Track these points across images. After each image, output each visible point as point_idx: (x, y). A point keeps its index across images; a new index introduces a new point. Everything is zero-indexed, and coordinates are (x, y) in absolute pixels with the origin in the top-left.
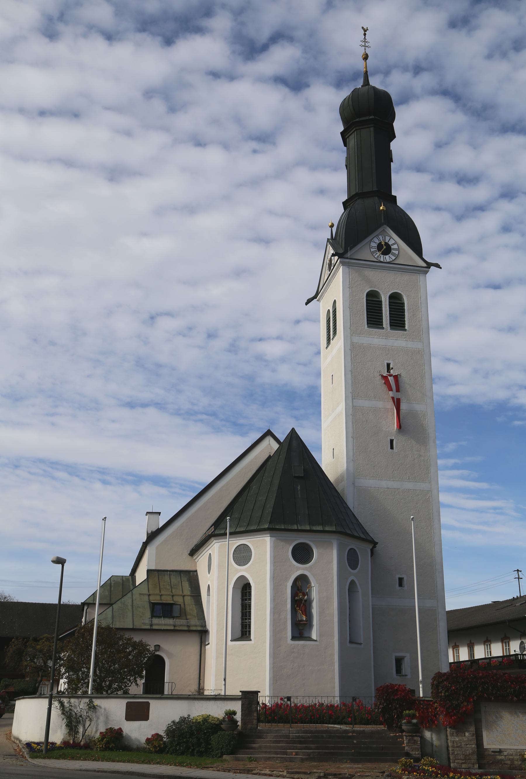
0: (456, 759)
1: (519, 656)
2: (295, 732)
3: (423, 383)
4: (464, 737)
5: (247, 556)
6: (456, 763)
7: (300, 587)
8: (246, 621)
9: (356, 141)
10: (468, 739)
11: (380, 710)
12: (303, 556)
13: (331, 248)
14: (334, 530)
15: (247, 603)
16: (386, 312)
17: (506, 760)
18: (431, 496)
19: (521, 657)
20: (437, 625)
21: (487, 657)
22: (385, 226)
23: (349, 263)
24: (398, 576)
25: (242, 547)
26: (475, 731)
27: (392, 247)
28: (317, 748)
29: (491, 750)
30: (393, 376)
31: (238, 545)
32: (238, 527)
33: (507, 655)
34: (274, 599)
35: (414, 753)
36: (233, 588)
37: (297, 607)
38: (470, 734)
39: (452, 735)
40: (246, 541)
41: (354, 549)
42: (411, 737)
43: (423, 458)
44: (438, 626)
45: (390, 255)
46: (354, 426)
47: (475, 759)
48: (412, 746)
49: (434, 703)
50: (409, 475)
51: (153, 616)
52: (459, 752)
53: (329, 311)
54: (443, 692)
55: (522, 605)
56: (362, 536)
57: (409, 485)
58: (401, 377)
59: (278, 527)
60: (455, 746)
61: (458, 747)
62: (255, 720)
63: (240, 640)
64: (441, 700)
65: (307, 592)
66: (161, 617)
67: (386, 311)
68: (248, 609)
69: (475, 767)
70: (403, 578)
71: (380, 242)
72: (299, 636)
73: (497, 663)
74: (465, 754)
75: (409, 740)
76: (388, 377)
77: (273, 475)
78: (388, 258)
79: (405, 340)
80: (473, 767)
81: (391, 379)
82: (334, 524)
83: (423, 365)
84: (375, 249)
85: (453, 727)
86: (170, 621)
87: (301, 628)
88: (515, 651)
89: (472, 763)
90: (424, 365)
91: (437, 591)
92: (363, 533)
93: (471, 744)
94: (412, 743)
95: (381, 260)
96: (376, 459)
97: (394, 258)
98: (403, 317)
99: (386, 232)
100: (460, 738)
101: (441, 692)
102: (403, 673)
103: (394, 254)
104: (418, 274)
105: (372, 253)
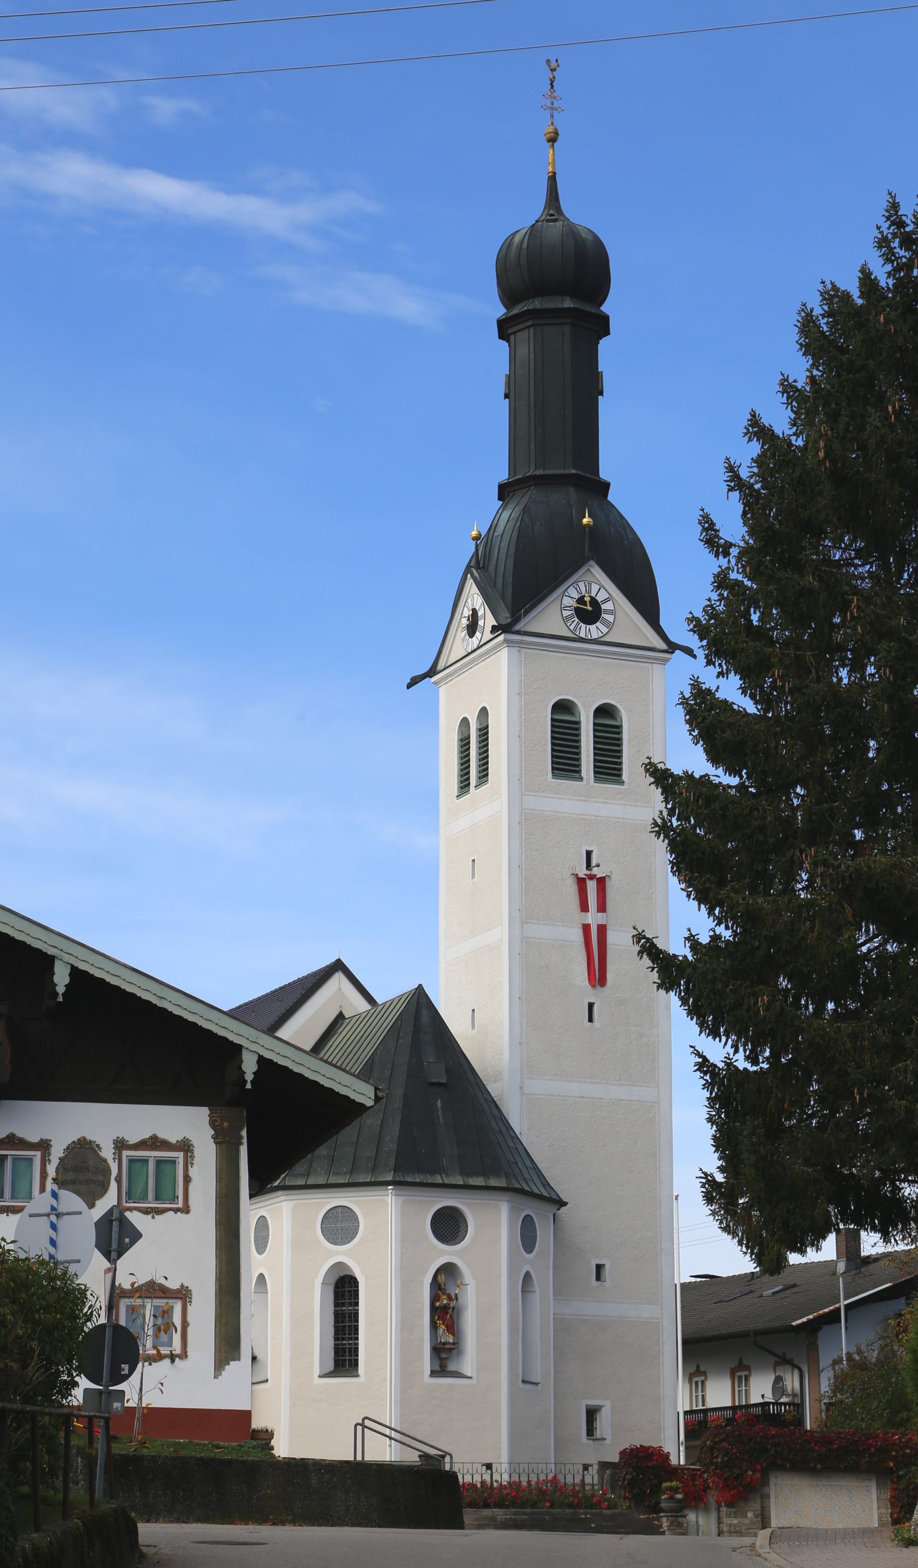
1: (771, 1408)
2: (501, 1514)
3: (651, 892)
4: (745, 1519)
5: (349, 1228)
7: (443, 1284)
8: (344, 1342)
9: (532, 350)
10: (751, 1521)
11: (626, 1482)
12: (450, 1230)
13: (475, 589)
14: (505, 1185)
15: (345, 1310)
16: (588, 745)
18: (659, 1113)
19: (775, 1408)
20: (659, 1351)
21: (695, 1408)
23: (521, 642)
25: (340, 1211)
27: (603, 607)
30: (597, 879)
31: (331, 1207)
32: (331, 1174)
33: (741, 1404)
36: (322, 1283)
37: (438, 1319)
38: (754, 1514)
39: (729, 1516)
40: (349, 1201)
41: (532, 1217)
42: (674, 1518)
44: (661, 1352)
45: (598, 624)
46: (524, 977)
49: (704, 1473)
50: (620, 1073)
53: (465, 722)
54: (720, 1456)
55: (777, 1296)
56: (545, 1194)
58: (610, 880)
59: (409, 1180)
63: (216, 1366)
64: (716, 1468)
65: (456, 1295)
67: (587, 742)
68: (347, 1321)
70: (604, 1265)
71: (580, 596)
72: (440, 1369)
73: (722, 1422)
77: (390, 1077)
78: (595, 631)
79: (622, 804)
82: (504, 1174)
83: (653, 854)
84: (572, 612)
85: (730, 1505)
87: (444, 1355)
88: (763, 1396)
90: (655, 855)
91: (661, 1290)
92: (544, 1186)
94: (676, 1526)
95: (581, 635)
96: (561, 1041)
98: (619, 754)
101: (717, 1457)
102: (598, 1434)
103: (606, 623)
105: (565, 620)
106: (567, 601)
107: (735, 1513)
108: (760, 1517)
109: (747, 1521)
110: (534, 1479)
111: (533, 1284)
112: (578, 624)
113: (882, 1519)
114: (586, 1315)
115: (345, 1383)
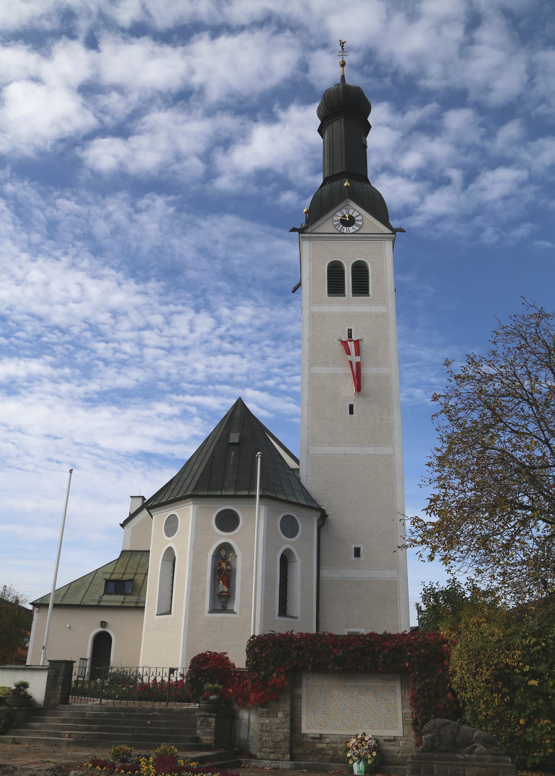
0: (263, 747)
4: (276, 719)
6: (263, 752)
17: (328, 749)
20: (397, 598)
22: (348, 200)
23: (309, 237)
24: (353, 547)
26: (289, 710)
27: (356, 219)
28: (100, 729)
29: (310, 736)
34: (193, 569)
35: (205, 738)
38: (284, 714)
42: (204, 718)
43: (385, 422)
45: (354, 226)
47: (287, 747)
48: (205, 729)
51: (106, 593)
52: (268, 738)
57: (370, 451)
60: (264, 730)
61: (267, 731)
62: (59, 694)
66: (113, 594)
67: (348, 279)
69: (286, 758)
74: (275, 741)
75: (202, 721)
76: (349, 342)
78: (351, 229)
80: (284, 757)
81: (351, 345)
86: (120, 598)
89: (283, 752)
91: (398, 561)
93: (283, 728)
94: (205, 726)
97: (357, 228)
99: (349, 205)
100: (271, 719)
104: (384, 241)
105: (335, 226)
106: (335, 218)
107: (267, 713)
108: (289, 717)
109: (277, 721)
110: (159, 680)
111: (295, 557)
112: (342, 227)
113: (407, 719)
114: (348, 578)
115: (166, 618)
